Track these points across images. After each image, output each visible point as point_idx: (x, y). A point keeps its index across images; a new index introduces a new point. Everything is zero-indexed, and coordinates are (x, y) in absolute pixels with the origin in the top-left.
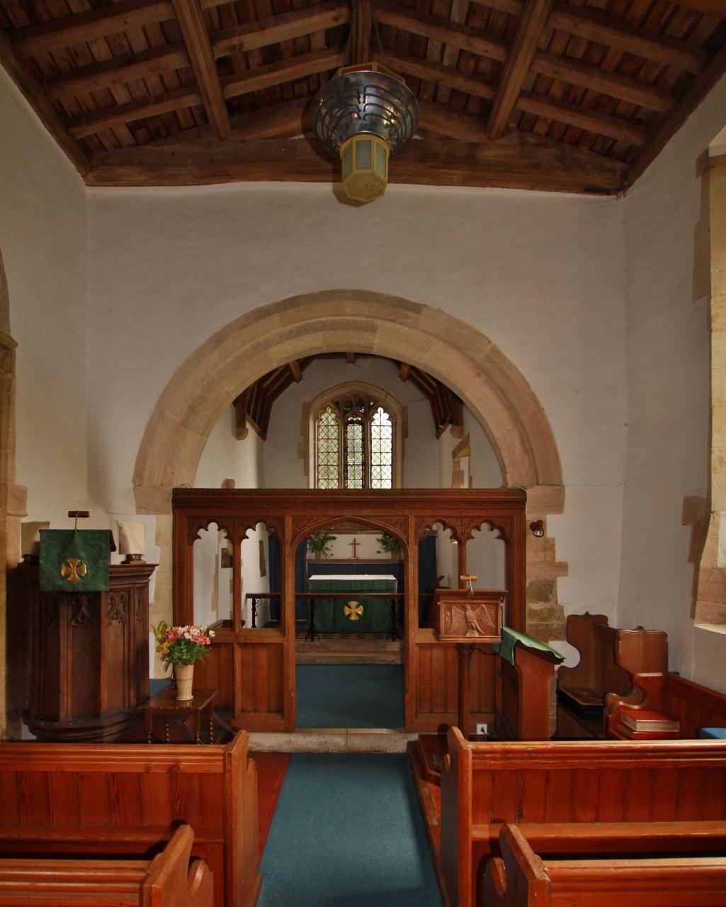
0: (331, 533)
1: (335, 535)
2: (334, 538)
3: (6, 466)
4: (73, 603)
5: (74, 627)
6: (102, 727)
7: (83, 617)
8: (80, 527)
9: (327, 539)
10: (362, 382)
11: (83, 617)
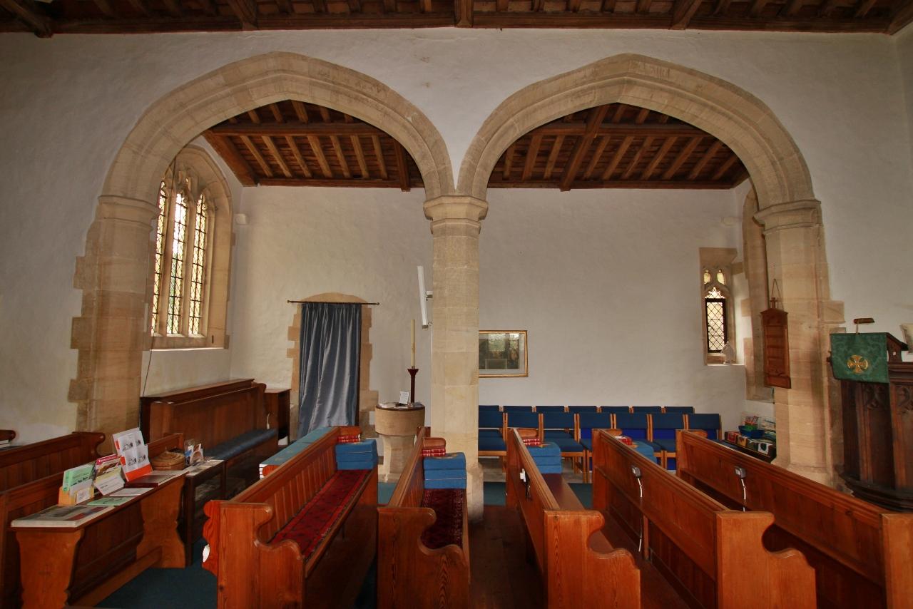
4: (867, 390)
7: (877, 402)
8: (861, 331)
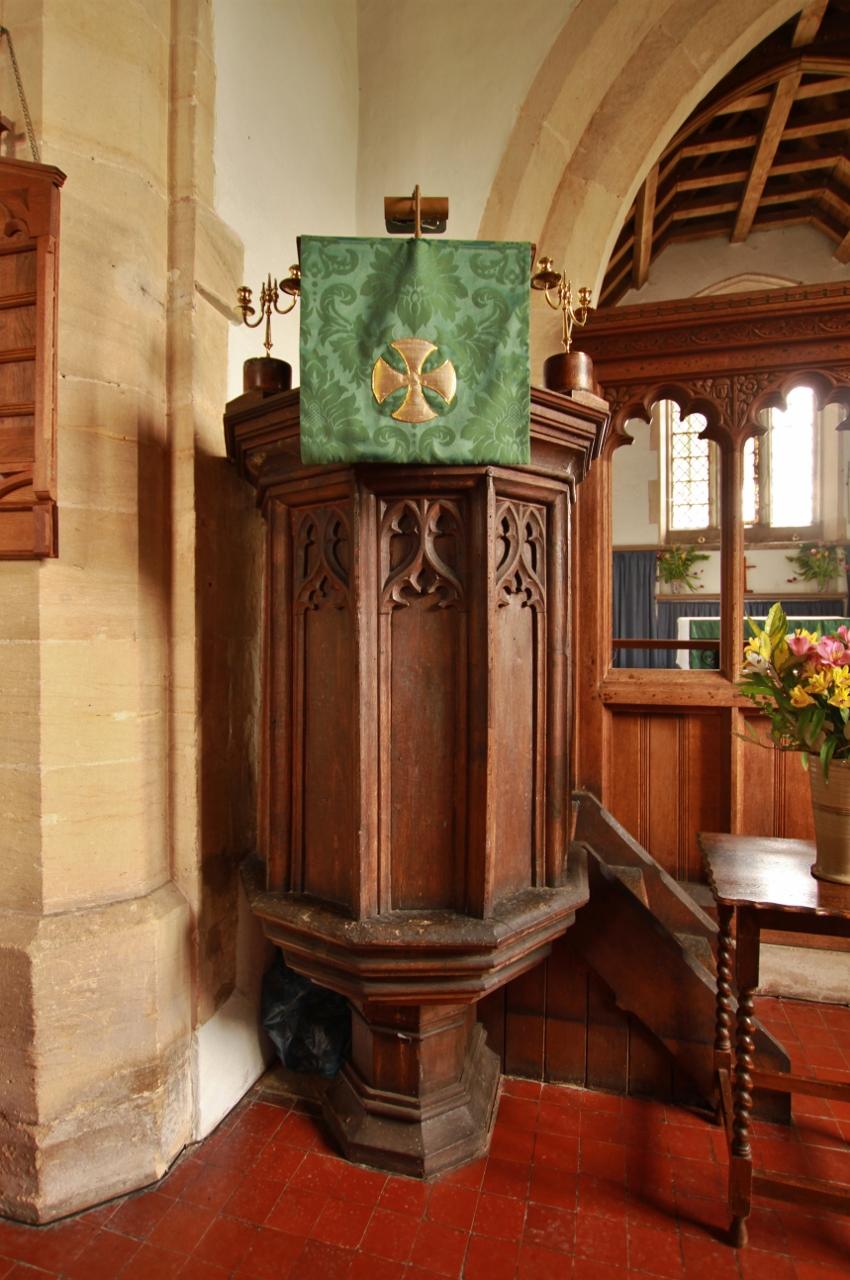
0: (701, 549)
1: (706, 553)
2: (705, 558)
3: (192, 147)
5: (397, 607)
6: (488, 949)
9: (692, 559)
10: (759, 274)
11: (427, 573)
